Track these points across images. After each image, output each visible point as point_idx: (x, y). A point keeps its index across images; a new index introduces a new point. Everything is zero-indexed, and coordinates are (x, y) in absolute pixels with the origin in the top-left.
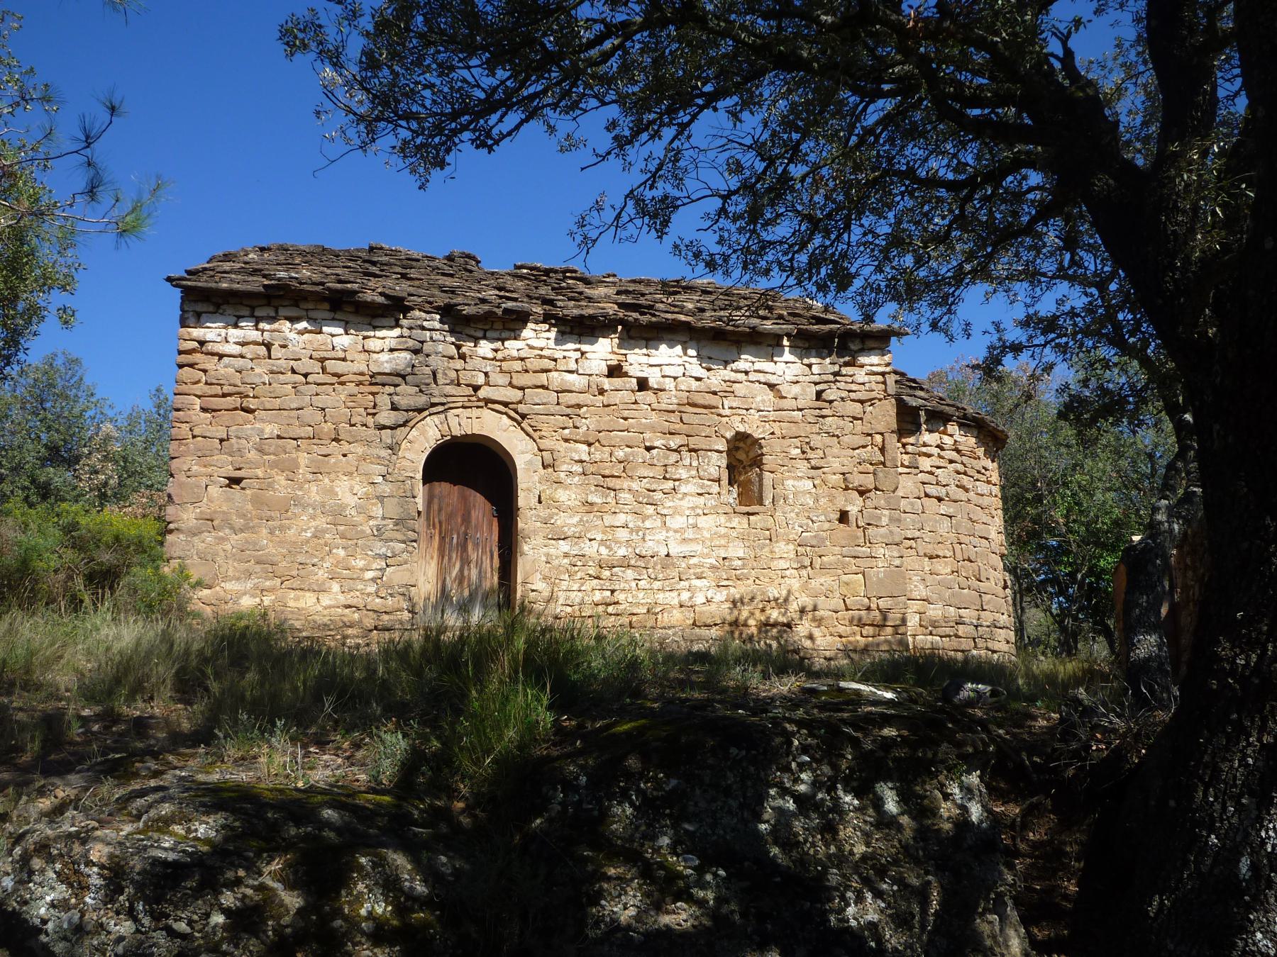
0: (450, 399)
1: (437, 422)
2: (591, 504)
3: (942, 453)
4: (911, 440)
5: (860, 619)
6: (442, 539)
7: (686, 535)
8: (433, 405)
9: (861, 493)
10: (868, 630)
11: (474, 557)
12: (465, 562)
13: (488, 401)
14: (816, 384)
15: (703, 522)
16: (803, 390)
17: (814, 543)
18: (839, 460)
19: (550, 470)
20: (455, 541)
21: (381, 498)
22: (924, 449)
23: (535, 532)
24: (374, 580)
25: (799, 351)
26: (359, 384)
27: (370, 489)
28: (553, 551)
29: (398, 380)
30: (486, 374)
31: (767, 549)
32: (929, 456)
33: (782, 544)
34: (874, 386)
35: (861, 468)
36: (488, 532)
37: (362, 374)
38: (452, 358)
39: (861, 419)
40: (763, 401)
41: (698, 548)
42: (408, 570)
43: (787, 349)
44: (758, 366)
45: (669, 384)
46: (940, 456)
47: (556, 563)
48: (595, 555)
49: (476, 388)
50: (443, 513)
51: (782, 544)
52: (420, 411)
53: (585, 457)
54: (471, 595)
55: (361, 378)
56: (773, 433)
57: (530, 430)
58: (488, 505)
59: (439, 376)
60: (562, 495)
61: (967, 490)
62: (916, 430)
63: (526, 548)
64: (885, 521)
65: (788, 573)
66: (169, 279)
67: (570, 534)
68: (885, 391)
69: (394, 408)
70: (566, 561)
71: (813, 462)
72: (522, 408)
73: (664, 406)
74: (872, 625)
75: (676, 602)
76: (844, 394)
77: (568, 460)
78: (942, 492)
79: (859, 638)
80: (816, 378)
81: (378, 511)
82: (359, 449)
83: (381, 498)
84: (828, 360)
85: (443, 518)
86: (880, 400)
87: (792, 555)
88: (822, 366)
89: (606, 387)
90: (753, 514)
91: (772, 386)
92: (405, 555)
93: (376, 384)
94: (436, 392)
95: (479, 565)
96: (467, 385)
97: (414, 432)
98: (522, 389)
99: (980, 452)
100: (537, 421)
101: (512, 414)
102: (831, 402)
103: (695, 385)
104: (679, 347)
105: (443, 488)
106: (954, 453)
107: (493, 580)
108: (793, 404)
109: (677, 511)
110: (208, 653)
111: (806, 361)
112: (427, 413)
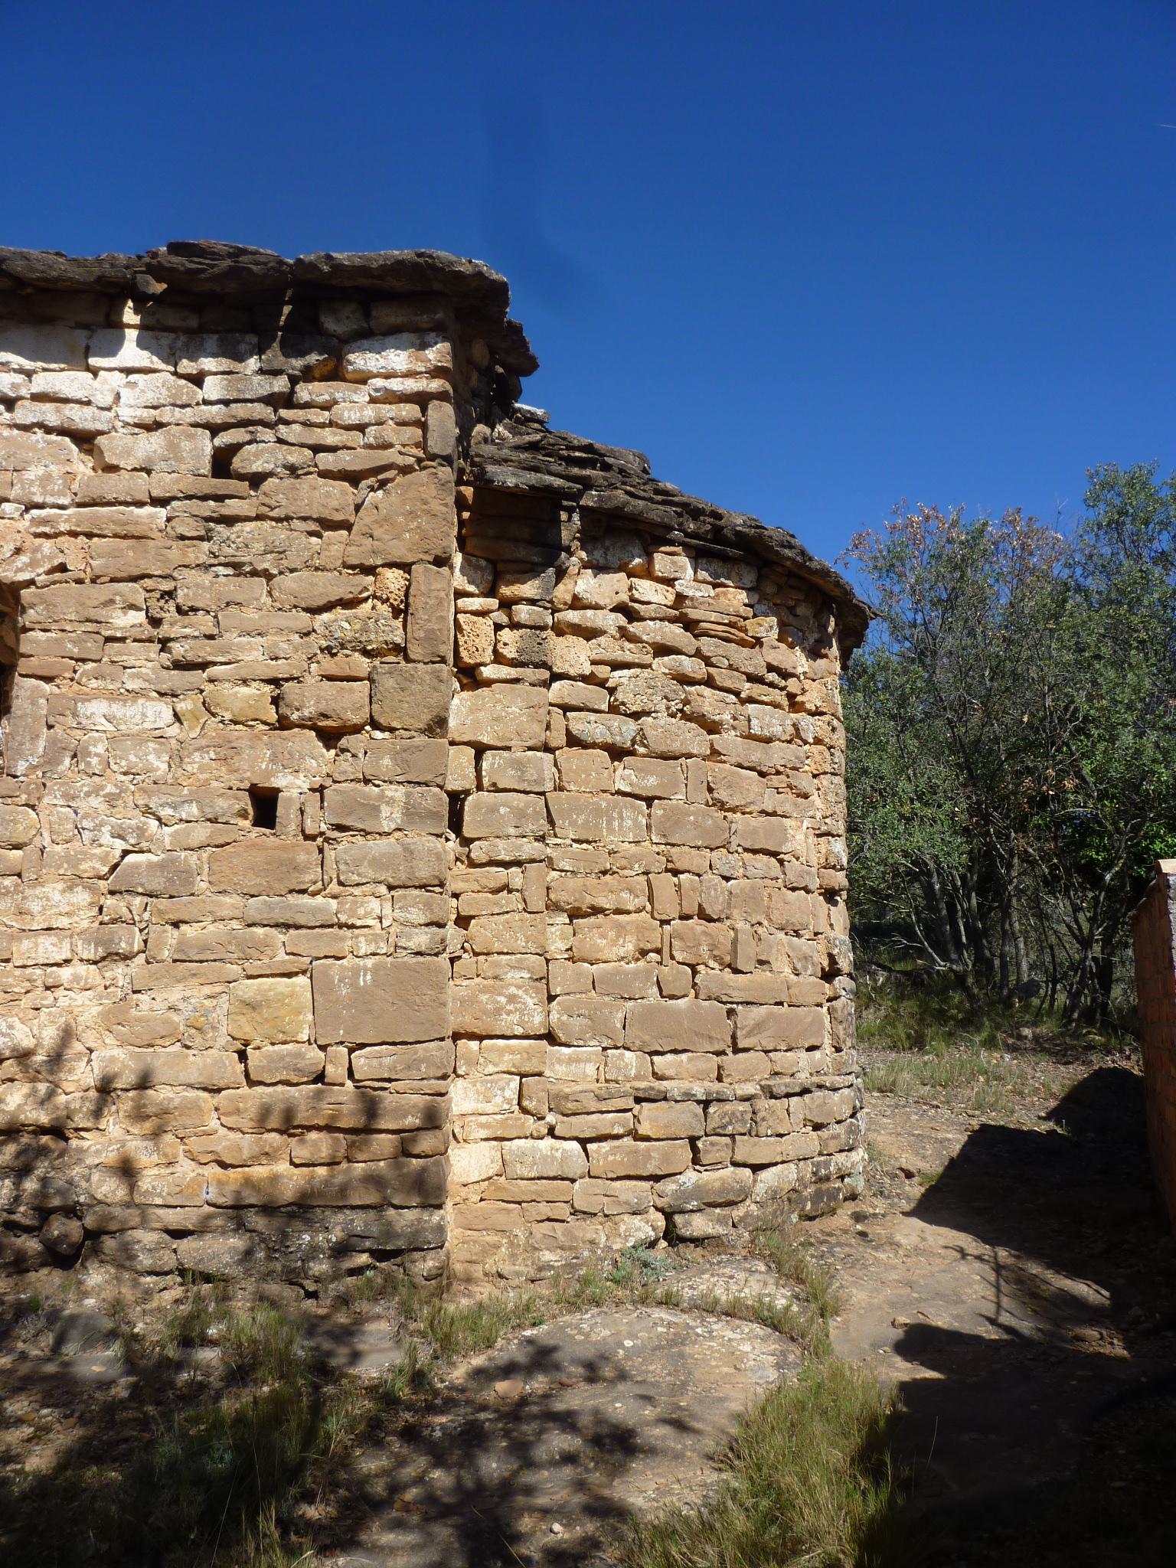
3: (634, 628)
4: (529, 589)
5: (289, 1115)
10: (320, 1144)
14: (215, 429)
16: (172, 446)
17: (156, 884)
18: (259, 640)
22: (572, 616)
25: (167, 339)
32: (590, 634)
33: (54, 891)
34: (390, 432)
35: (329, 665)
39: (347, 526)
40: (46, 479)
43: (131, 335)
44: (42, 382)
46: (624, 634)
51: (54, 891)
56: (63, 568)
61: (713, 728)
62: (546, 557)
64: (389, 817)
65: (65, 973)
68: (423, 445)
71: (178, 649)
74: (329, 1128)
76: (295, 457)
78: (624, 730)
79: (282, 1167)
80: (216, 413)
84: (253, 363)
86: (406, 470)
87: (85, 920)
88: (222, 379)
91: (85, 440)
99: (767, 627)
102: (256, 480)
106: (677, 629)
108: (142, 485)
110: (939, 843)
111: (186, 366)
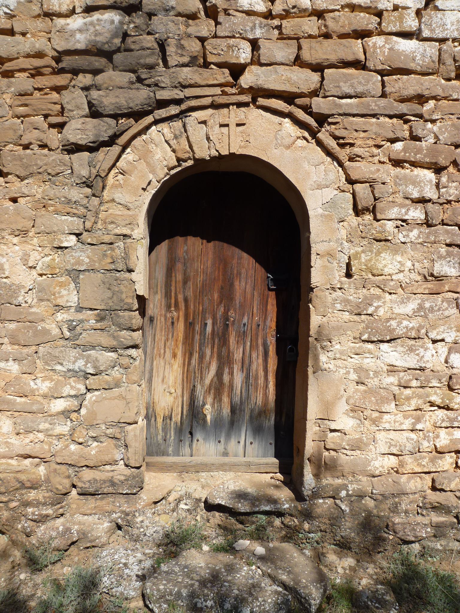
0: (189, 92)
1: (169, 136)
2: (438, 278)
6: (190, 326)
8: (162, 104)
11: (238, 355)
12: (225, 361)
13: (257, 93)
19: (368, 217)
20: (209, 329)
21: (74, 274)
23: (340, 329)
24: (66, 414)
26: (37, 73)
27: (57, 257)
28: (368, 362)
29: (99, 62)
30: (255, 44)
36: (262, 316)
37: (40, 55)
38: (193, 16)
42: (121, 397)
47: (373, 382)
48: (441, 367)
49: (237, 71)
50: (190, 284)
52: (137, 115)
53: (430, 193)
54: (233, 411)
55: (37, 62)
57: (332, 144)
58: (261, 271)
59: (171, 50)
60: (389, 263)
63: (323, 358)
67: (399, 332)
69: (95, 113)
70: (392, 380)
72: (319, 104)
77: (399, 199)
81: (70, 296)
82: (35, 188)
83: (74, 274)
85: (190, 294)
92: (116, 373)
93: (62, 71)
94: (165, 80)
95: (246, 366)
96: (220, 65)
97: (129, 156)
98: (318, 68)
100: (347, 128)
101: (301, 115)
105: (198, 252)
107: (266, 392)
112: (150, 119)
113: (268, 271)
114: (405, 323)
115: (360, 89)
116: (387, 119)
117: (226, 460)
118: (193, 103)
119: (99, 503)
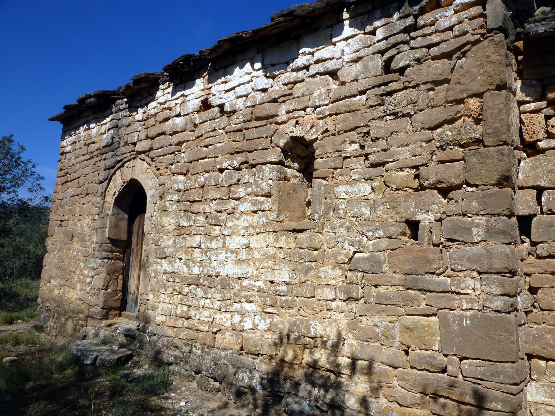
7: (240, 256)
9: (445, 192)
15: (256, 242)
31: (312, 274)
34: (466, 26)
35: (441, 155)
41: (249, 270)
44: (317, 56)
45: (240, 104)
51: (328, 268)
52: (113, 167)
64: (477, 234)
65: (334, 304)
66: (52, 120)
73: (234, 127)
75: (228, 324)
84: (396, 16)
87: (340, 282)
89: (197, 121)
90: (301, 231)
103: (260, 96)
104: (248, 65)
109: (234, 232)
112: (115, 168)
113: (509, 8)
114: (170, 249)
115: (161, 144)
116: (170, 155)
117: (139, 294)
118: (124, 160)
119: (94, 322)
